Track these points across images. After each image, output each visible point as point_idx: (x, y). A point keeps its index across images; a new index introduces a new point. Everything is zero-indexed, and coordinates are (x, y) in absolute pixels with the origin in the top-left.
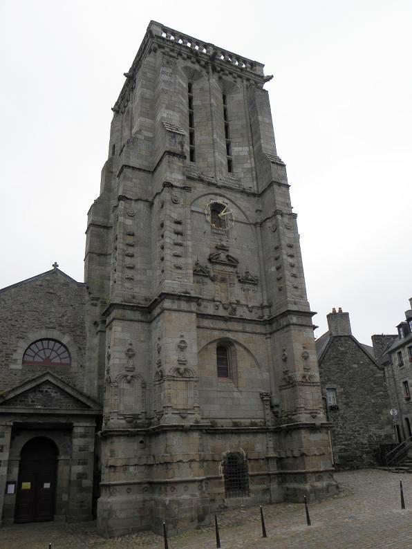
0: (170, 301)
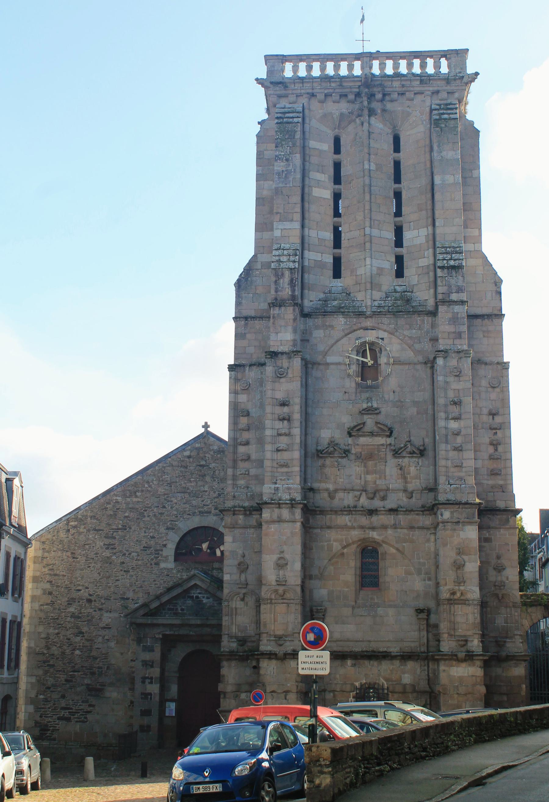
0: (269, 510)
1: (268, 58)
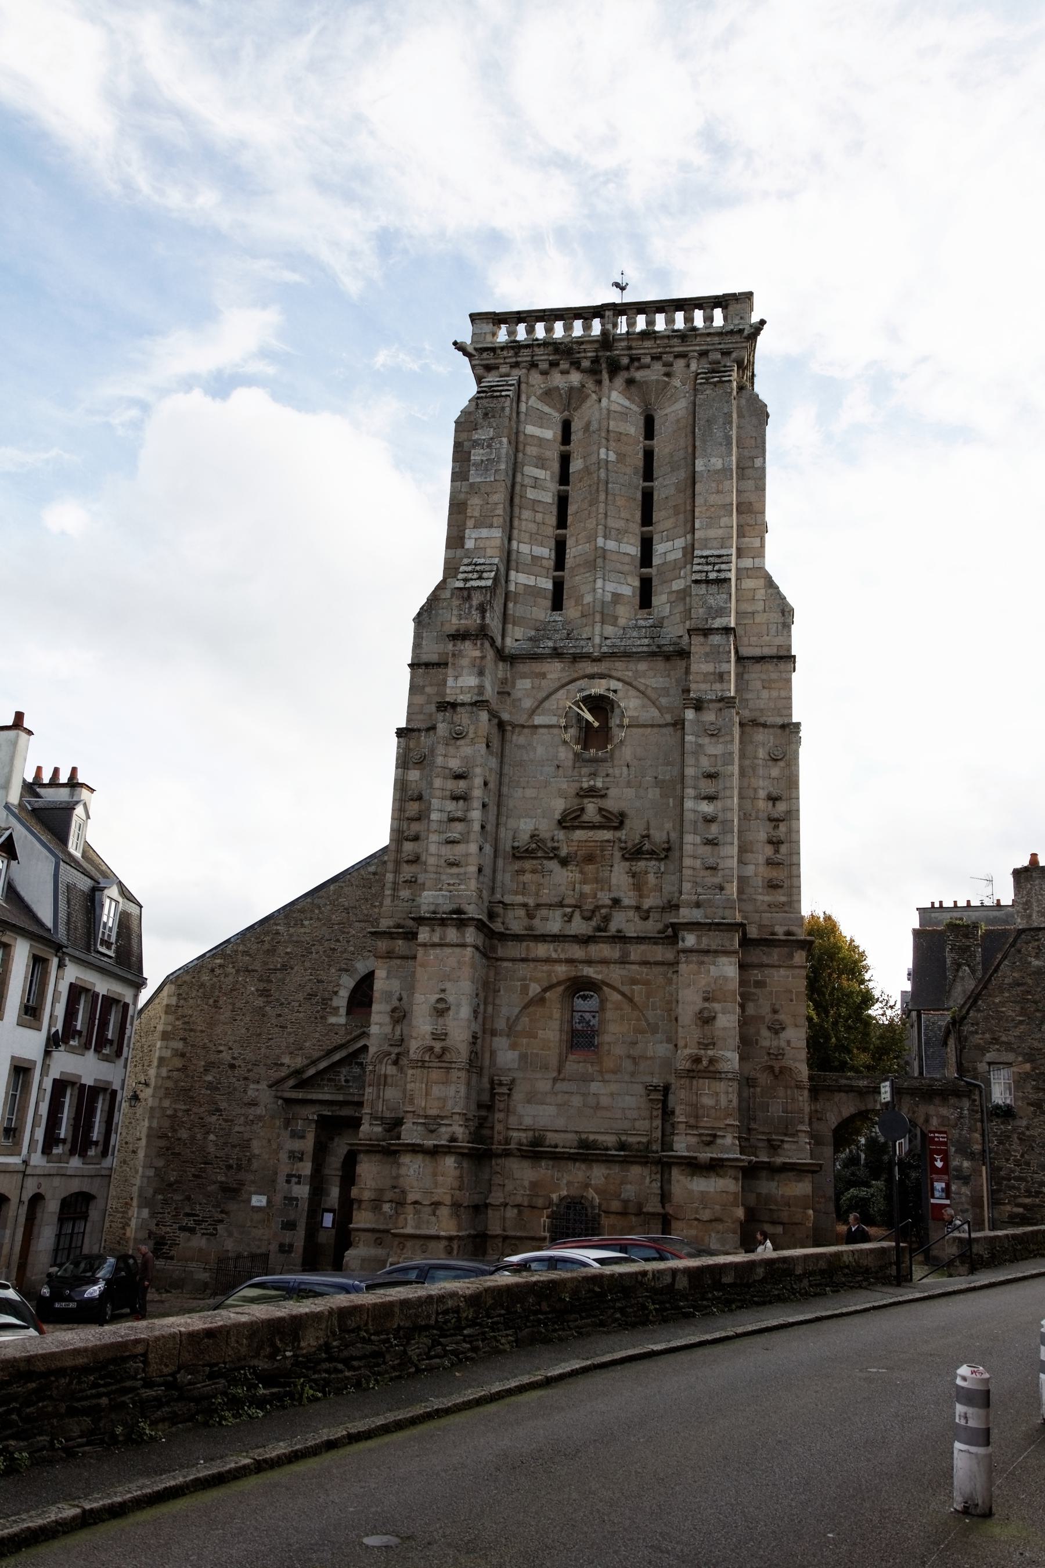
0: (427, 928)
1: (474, 317)
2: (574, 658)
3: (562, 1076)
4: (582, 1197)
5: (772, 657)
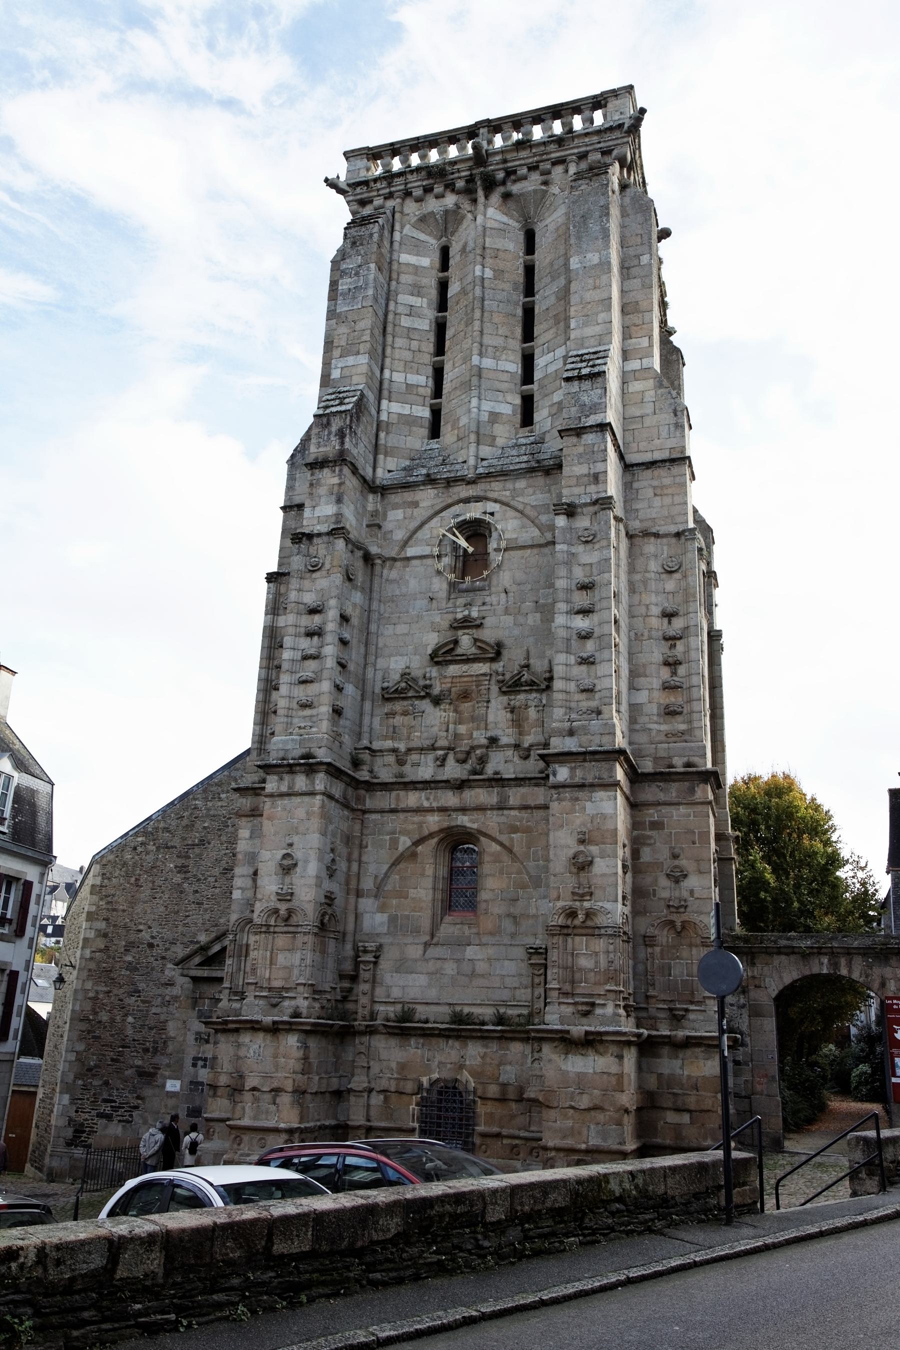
0: (276, 777)
1: (348, 155)
2: (448, 482)
3: (435, 940)
4: (456, 1080)
5: (663, 461)
